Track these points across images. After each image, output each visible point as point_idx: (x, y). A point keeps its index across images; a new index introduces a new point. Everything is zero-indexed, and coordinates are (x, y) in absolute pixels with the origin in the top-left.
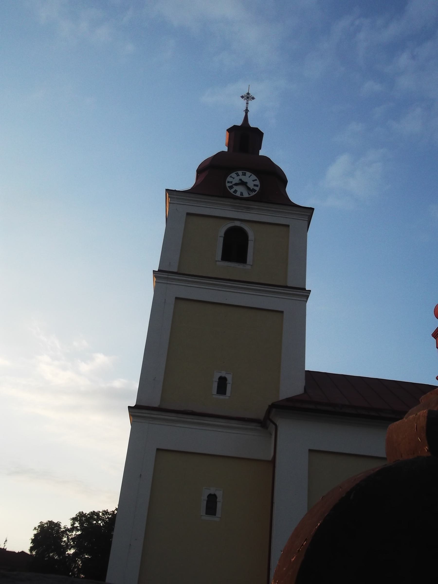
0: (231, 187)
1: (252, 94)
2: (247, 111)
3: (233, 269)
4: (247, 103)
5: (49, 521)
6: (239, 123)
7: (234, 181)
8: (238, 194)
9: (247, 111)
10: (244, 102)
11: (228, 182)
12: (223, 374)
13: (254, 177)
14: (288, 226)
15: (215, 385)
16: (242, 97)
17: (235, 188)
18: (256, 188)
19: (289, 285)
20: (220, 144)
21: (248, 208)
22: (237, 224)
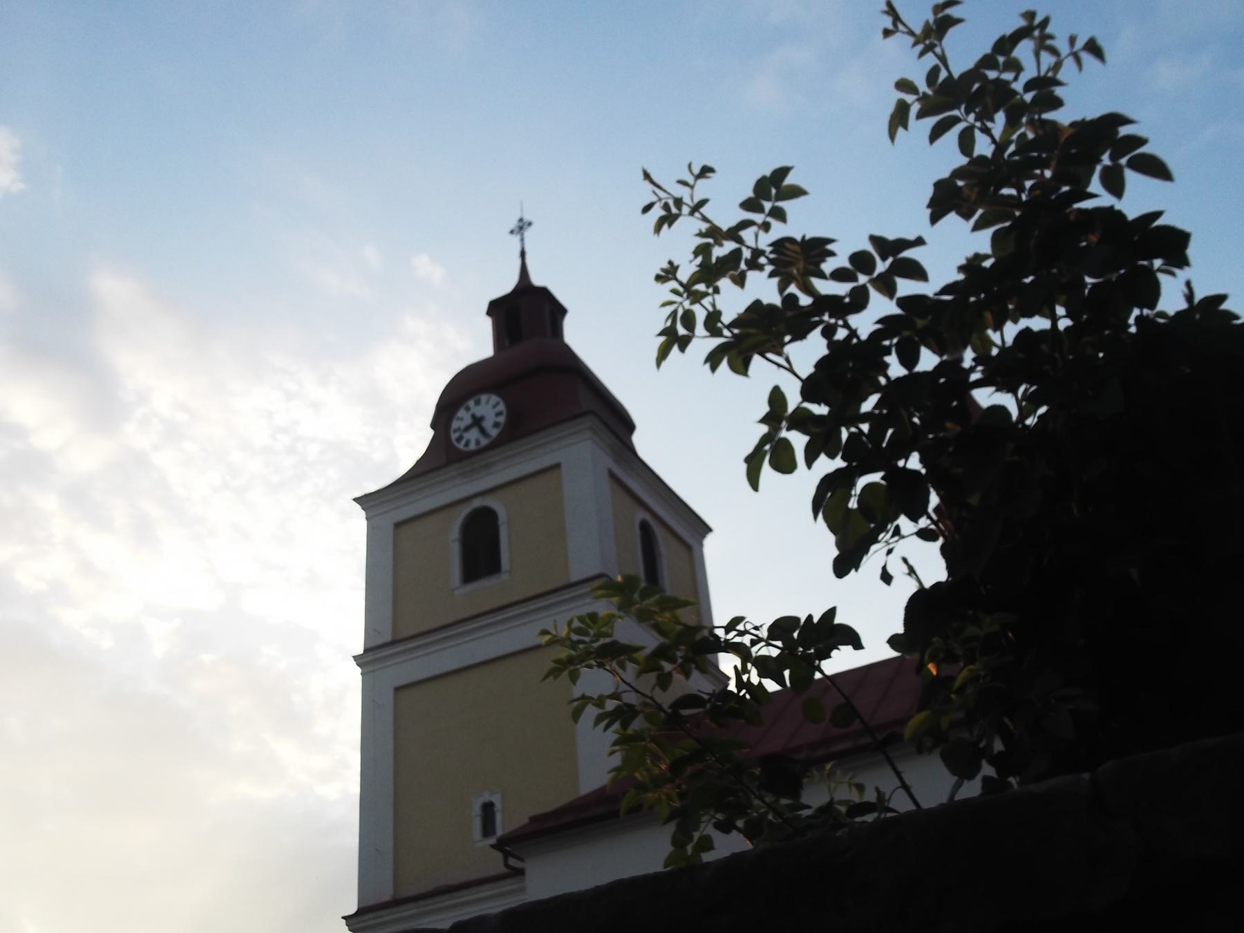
0: (459, 439)
1: (527, 218)
2: (523, 254)
3: (487, 590)
4: (522, 240)
5: (929, 206)
6: (506, 284)
7: (463, 425)
8: (472, 447)
9: (523, 254)
10: (516, 239)
11: (455, 431)
12: (487, 797)
13: (494, 399)
14: (557, 466)
15: (477, 824)
16: (512, 232)
17: (467, 436)
18: (463, 442)
19: (574, 578)
20: (476, 343)
21: (488, 466)
22: (477, 503)
